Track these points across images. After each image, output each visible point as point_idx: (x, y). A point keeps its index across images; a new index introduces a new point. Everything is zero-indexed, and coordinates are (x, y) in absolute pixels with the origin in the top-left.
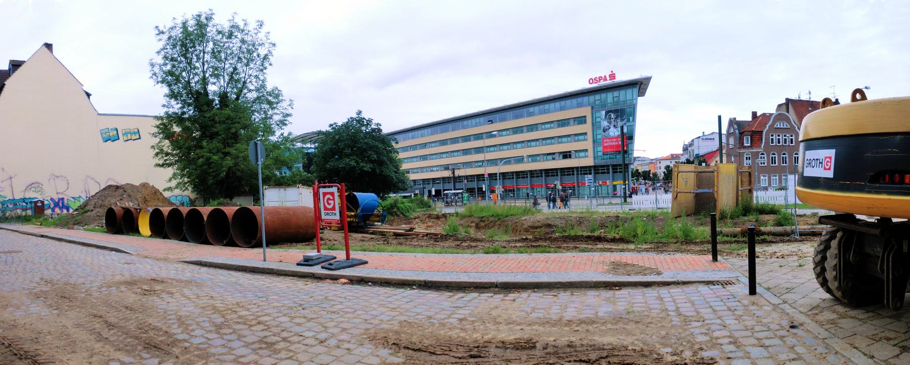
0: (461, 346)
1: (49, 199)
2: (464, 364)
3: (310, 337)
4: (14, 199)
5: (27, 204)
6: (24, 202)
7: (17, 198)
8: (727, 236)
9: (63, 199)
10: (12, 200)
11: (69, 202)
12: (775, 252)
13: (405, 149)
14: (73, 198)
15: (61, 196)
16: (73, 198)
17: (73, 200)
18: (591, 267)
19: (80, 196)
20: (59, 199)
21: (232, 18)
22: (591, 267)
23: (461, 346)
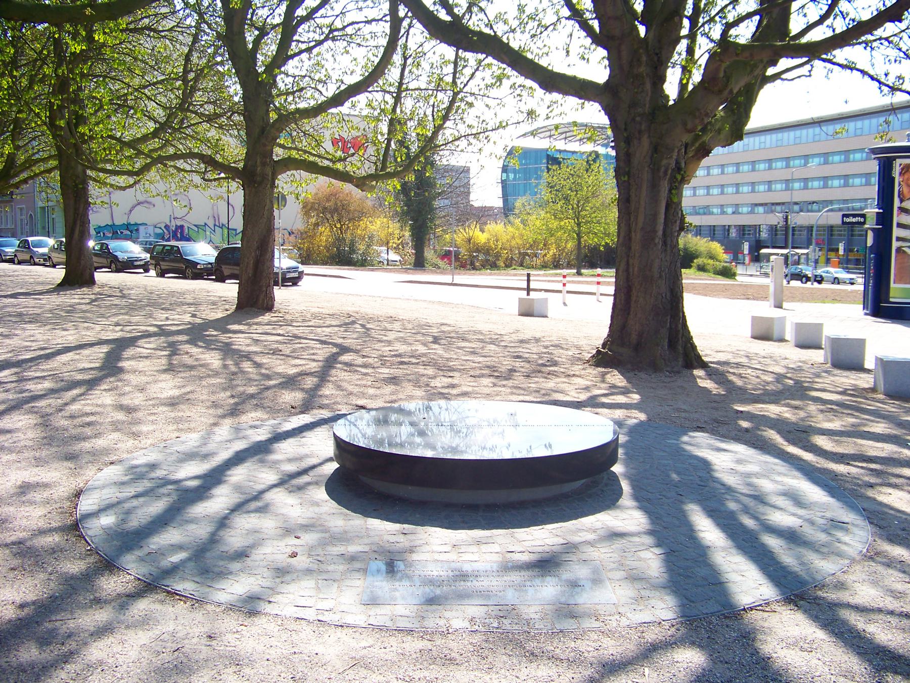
0: (369, 22)
1: (163, 226)
2: (369, 3)
3: (858, 70)
4: (114, 224)
5: (131, 232)
6: (128, 229)
7: (118, 222)
8: (309, 484)
9: (182, 227)
10: (111, 226)
11: (191, 232)
12: (431, 408)
13: (608, 284)
14: (196, 226)
15: (179, 223)
16: (196, 226)
17: (196, 229)
18: (355, 425)
19: (206, 224)
20: (177, 227)
21: (345, 54)
22: (355, 425)
23: (369, 22)
